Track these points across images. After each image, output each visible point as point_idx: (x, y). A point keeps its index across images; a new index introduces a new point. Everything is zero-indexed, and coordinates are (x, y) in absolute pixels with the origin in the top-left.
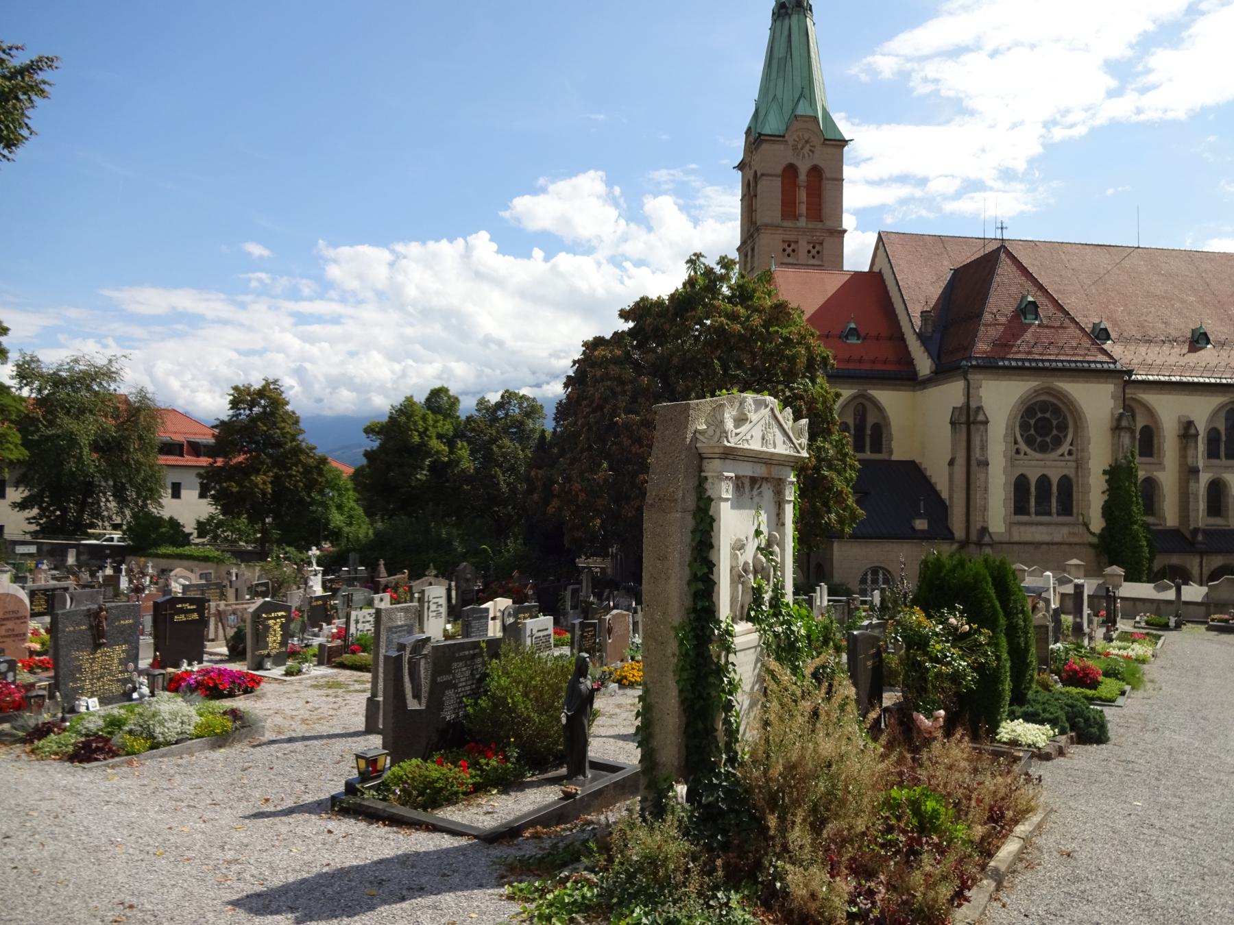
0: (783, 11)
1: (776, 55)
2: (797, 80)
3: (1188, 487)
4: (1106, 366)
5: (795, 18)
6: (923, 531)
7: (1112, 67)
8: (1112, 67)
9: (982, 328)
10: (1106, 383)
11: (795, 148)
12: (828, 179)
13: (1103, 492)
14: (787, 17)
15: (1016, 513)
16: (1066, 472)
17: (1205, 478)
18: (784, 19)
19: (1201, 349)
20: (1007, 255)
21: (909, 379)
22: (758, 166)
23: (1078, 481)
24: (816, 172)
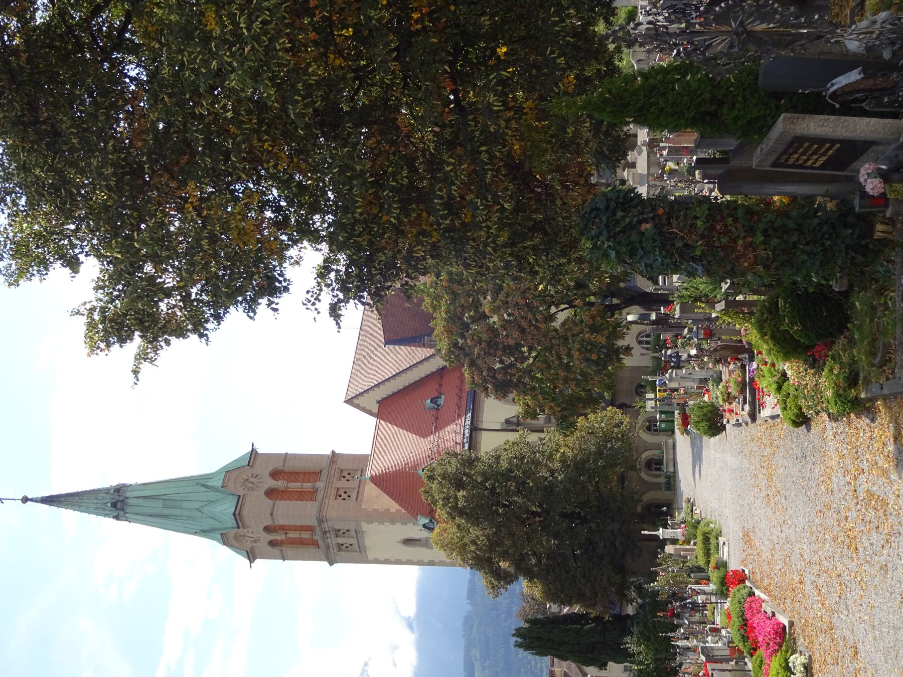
0: (119, 505)
2: (187, 490)
12: (284, 466)
14: (126, 500)
18: (128, 505)
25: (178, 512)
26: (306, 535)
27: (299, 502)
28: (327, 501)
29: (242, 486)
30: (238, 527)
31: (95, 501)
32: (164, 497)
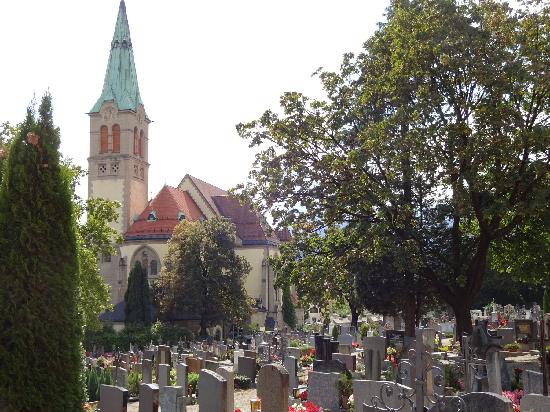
0: (124, 45)
25: (123, 77)
26: (110, 147)
30: (119, 110)
31: (126, 32)
32: (131, 71)
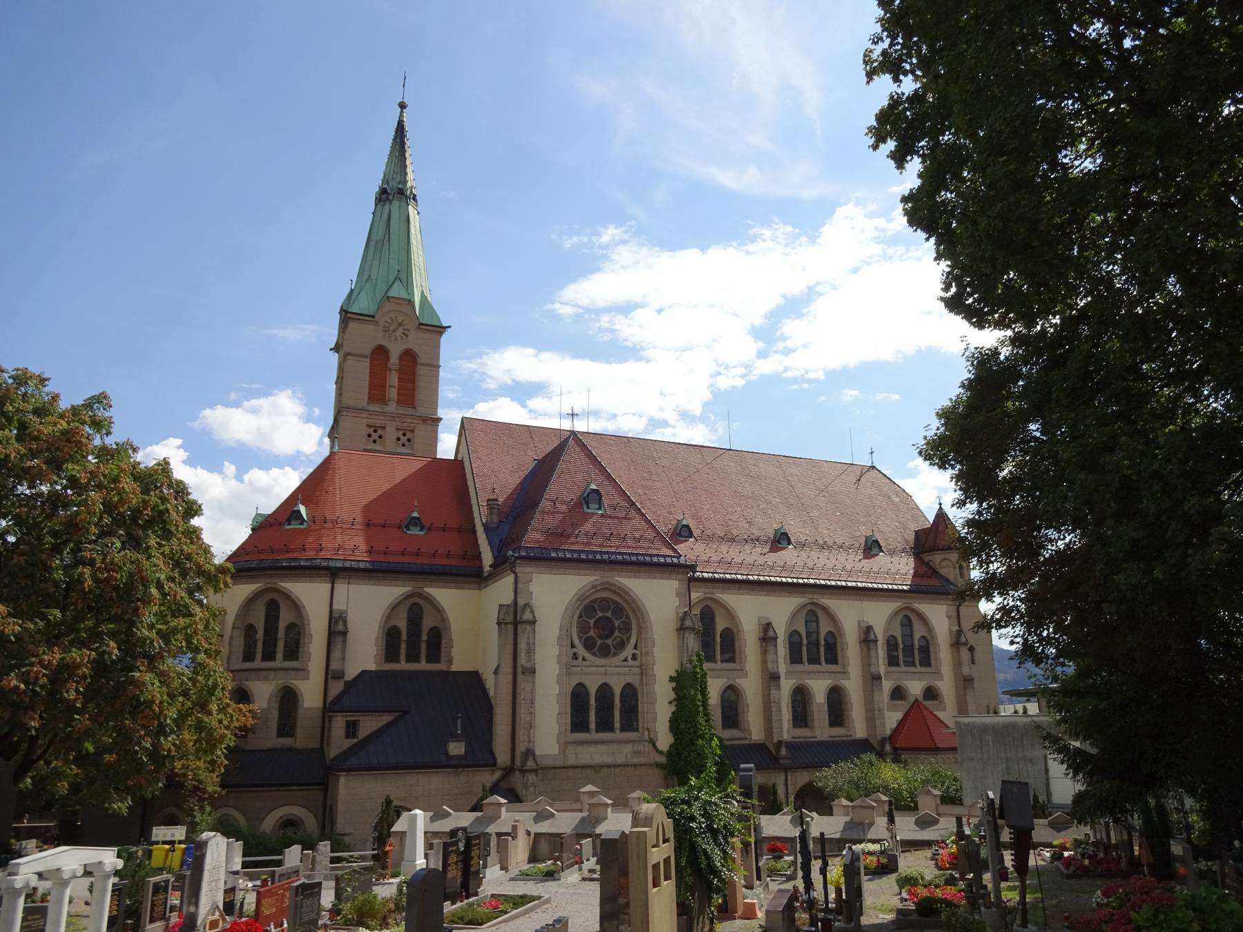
1: (374, 238)
3: (769, 694)
4: (668, 560)
5: (395, 204)
6: (459, 757)
7: (756, 332)
8: (756, 332)
9: (537, 516)
10: (670, 579)
11: (386, 330)
12: (423, 364)
13: (670, 703)
14: (388, 202)
15: (572, 731)
16: (629, 679)
17: (787, 686)
19: (783, 549)
20: (576, 442)
21: (474, 576)
22: (346, 349)
23: (643, 690)
24: (409, 357)
27: (367, 384)
28: (364, 416)
29: (392, 320)
